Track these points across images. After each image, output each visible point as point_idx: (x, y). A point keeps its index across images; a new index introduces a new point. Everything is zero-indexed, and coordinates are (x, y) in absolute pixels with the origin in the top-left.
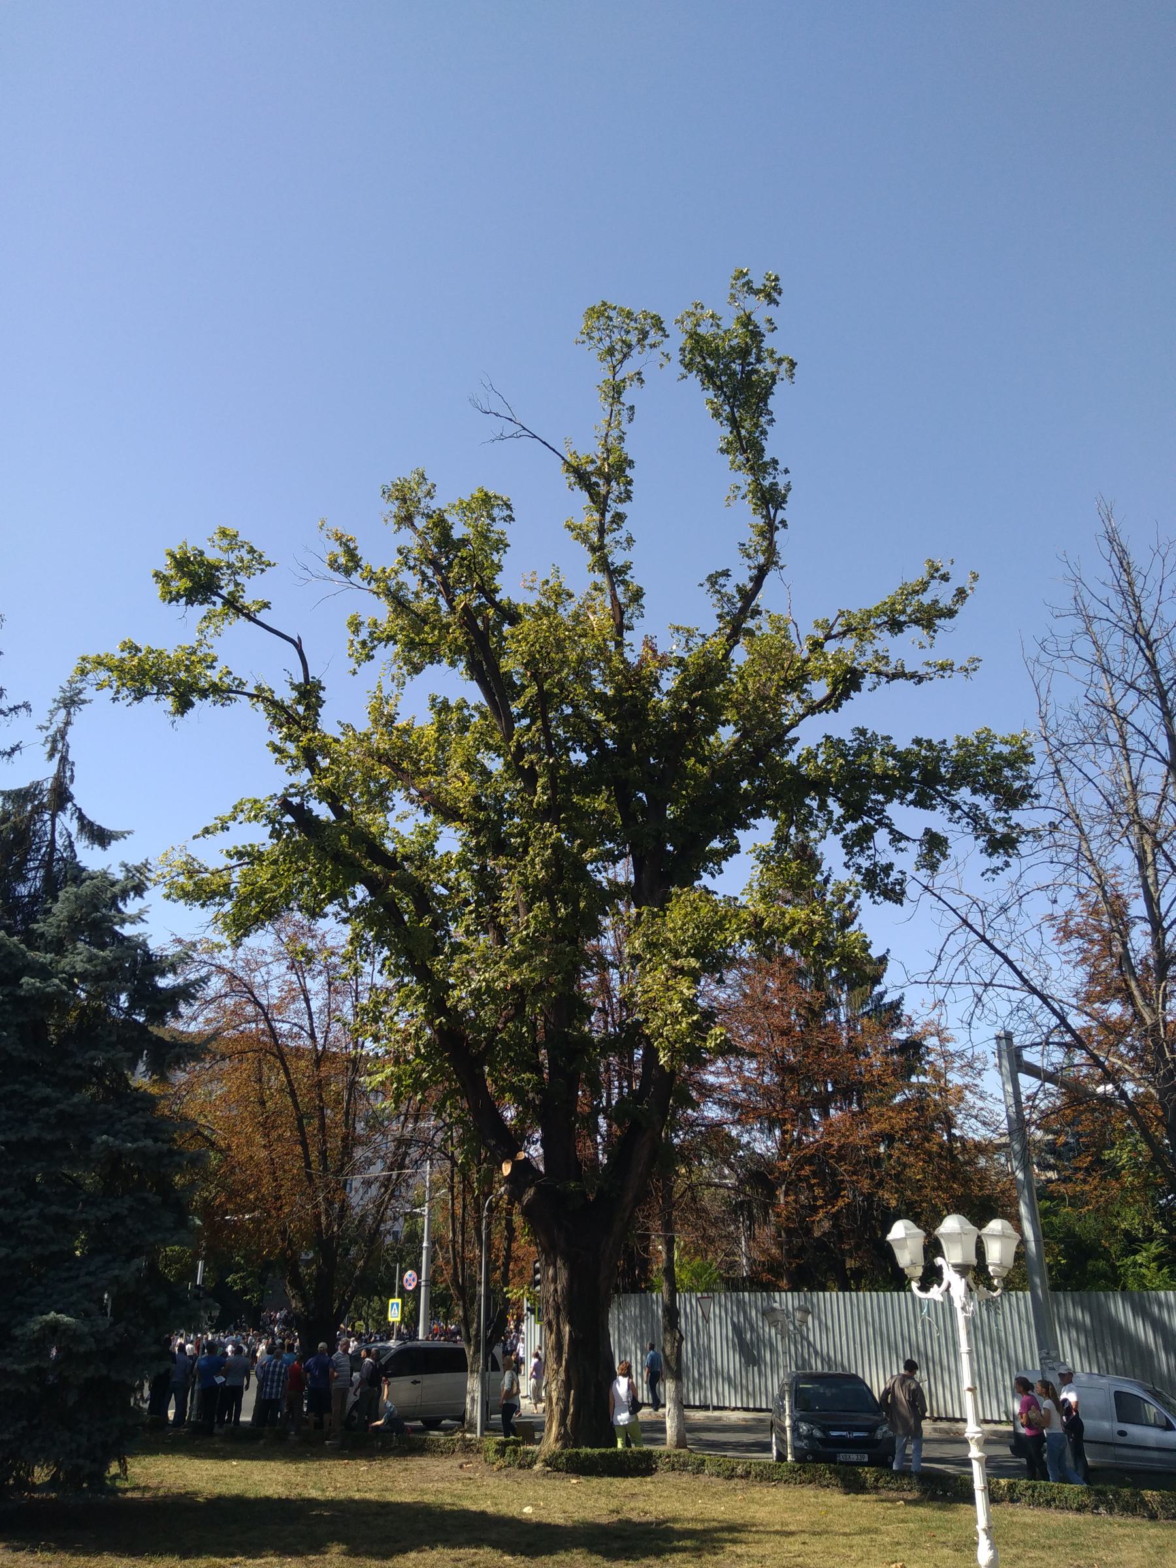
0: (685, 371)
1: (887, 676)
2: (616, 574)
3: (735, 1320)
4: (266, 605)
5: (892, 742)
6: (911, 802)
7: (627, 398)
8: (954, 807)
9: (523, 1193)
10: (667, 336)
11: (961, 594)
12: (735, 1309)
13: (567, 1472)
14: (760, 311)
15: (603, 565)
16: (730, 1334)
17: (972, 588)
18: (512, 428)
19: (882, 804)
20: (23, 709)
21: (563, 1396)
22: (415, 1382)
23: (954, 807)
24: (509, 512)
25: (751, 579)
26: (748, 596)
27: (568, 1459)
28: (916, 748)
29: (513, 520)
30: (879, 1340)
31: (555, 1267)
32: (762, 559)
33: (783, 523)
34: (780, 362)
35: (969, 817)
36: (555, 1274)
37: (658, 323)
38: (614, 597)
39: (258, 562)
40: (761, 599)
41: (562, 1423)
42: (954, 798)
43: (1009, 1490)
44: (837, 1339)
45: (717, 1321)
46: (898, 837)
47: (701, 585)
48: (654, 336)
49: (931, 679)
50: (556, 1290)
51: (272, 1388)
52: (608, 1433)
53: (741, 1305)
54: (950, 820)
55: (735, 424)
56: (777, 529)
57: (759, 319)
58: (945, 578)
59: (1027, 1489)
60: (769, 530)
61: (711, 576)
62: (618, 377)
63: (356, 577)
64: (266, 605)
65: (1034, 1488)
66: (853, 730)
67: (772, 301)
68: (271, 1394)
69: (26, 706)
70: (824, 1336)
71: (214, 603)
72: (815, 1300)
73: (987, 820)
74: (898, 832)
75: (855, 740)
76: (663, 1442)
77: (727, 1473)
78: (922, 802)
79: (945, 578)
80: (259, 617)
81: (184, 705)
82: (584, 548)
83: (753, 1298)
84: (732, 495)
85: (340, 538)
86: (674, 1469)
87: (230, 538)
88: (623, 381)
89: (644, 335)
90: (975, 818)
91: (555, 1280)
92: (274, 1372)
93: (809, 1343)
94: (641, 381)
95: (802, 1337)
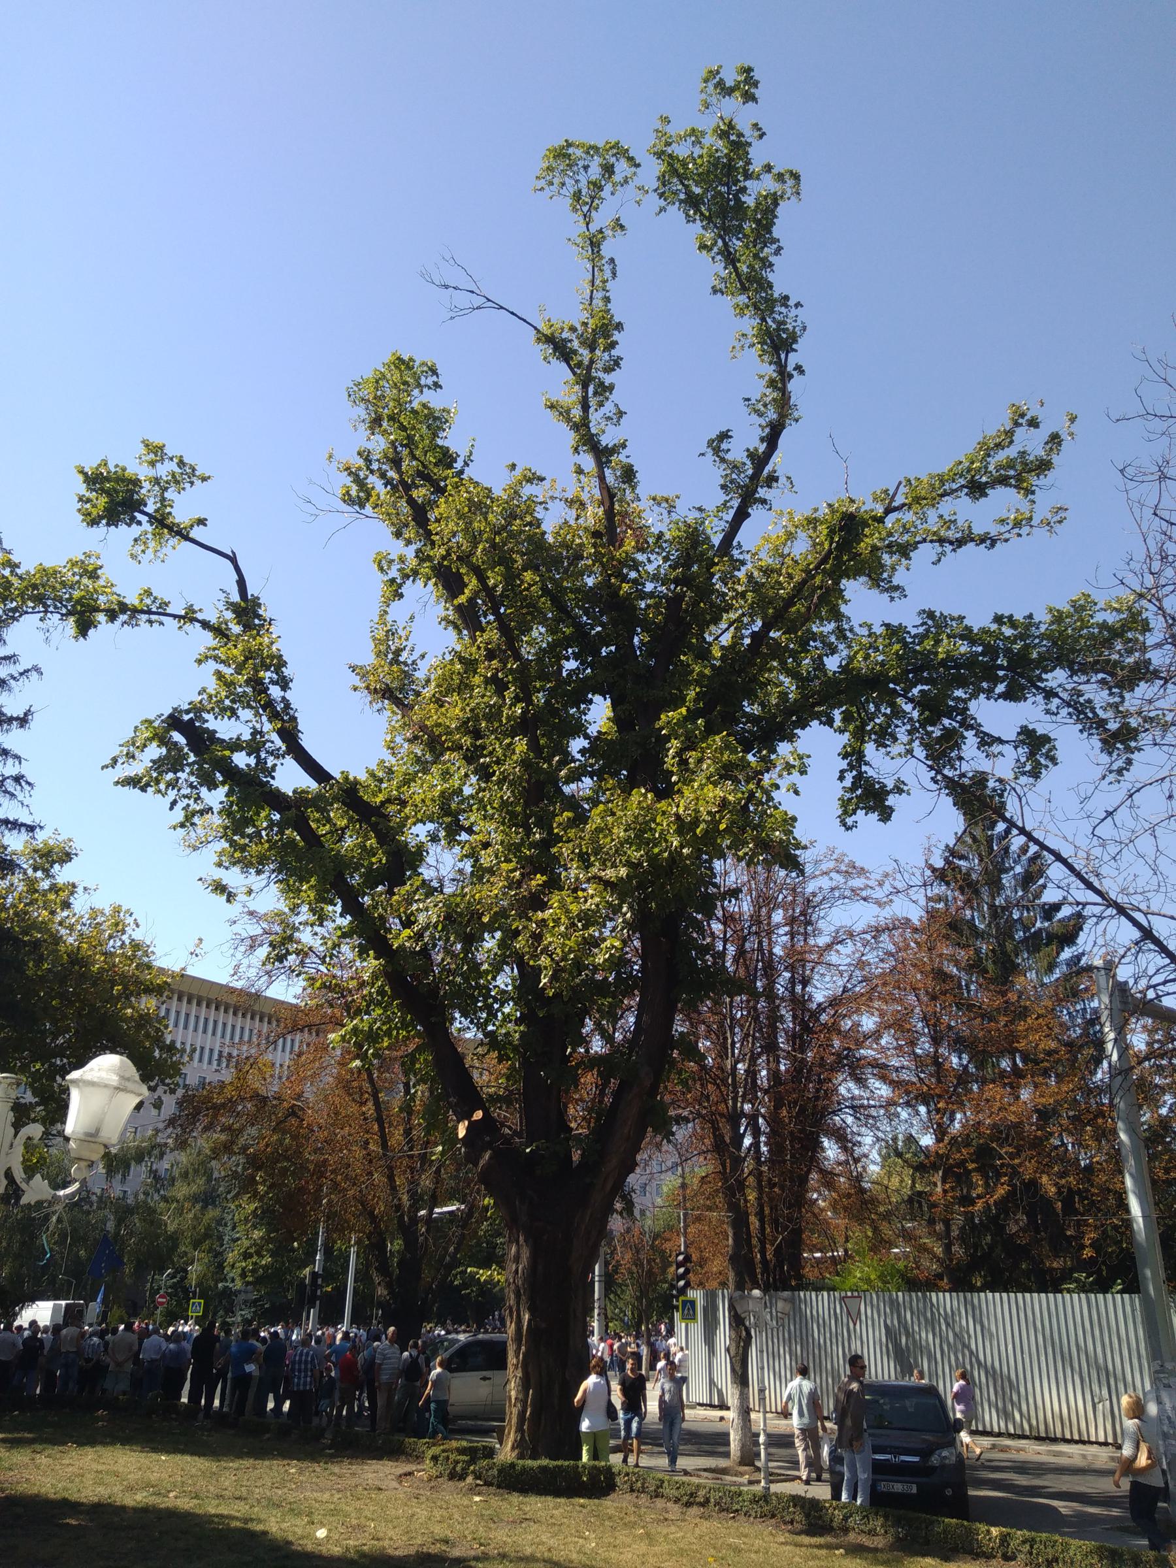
0: (662, 203)
1: (951, 543)
2: (603, 455)
3: (889, 1322)
4: (202, 522)
5: (966, 622)
6: (1000, 696)
7: (607, 250)
8: (1049, 694)
9: (480, 1157)
10: (638, 166)
11: (1055, 439)
12: (888, 1310)
13: (499, 1487)
14: (744, 117)
15: (589, 441)
16: (884, 1339)
17: (1071, 434)
18: (480, 301)
19: (965, 701)
20: (34, 673)
21: (521, 1396)
22: (484, 1379)
23: (1049, 694)
24: (434, 378)
25: (762, 440)
26: (760, 461)
27: (500, 1471)
28: (994, 627)
29: (441, 387)
30: (1050, 1350)
31: (518, 1244)
32: (772, 414)
33: (799, 368)
34: (780, 177)
35: (1069, 705)
36: (518, 1252)
37: (621, 152)
38: (602, 478)
39: (186, 475)
40: (778, 462)
41: (520, 1429)
42: (1049, 684)
43: (1002, 1544)
44: (1003, 1348)
45: (870, 1322)
46: (987, 741)
47: (703, 454)
48: (622, 168)
49: (1006, 540)
50: (517, 1271)
51: (299, 1378)
52: (570, 1443)
53: (894, 1305)
54: (1048, 712)
55: (730, 259)
56: (791, 376)
57: (744, 125)
58: (1034, 423)
59: (1024, 1542)
60: (781, 380)
61: (710, 443)
62: (594, 227)
63: (368, 509)
64: (202, 522)
65: (1032, 1542)
66: (919, 614)
67: (749, 97)
68: (298, 1384)
69: (36, 669)
70: (987, 1344)
71: (139, 523)
72: (976, 1301)
73: (1093, 710)
74: (986, 734)
75: (922, 625)
76: (727, 1455)
77: (685, 1499)
78: (1013, 695)
79: (1034, 423)
80: (192, 535)
81: (84, 627)
82: (564, 427)
83: (907, 1298)
84: (736, 344)
85: (347, 469)
86: (632, 1490)
87: (156, 452)
88: (601, 231)
89: (609, 170)
90: (1081, 710)
91: (517, 1259)
92: (306, 1361)
93: (971, 1353)
94: (622, 227)
95: (964, 1345)
